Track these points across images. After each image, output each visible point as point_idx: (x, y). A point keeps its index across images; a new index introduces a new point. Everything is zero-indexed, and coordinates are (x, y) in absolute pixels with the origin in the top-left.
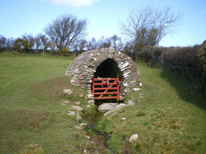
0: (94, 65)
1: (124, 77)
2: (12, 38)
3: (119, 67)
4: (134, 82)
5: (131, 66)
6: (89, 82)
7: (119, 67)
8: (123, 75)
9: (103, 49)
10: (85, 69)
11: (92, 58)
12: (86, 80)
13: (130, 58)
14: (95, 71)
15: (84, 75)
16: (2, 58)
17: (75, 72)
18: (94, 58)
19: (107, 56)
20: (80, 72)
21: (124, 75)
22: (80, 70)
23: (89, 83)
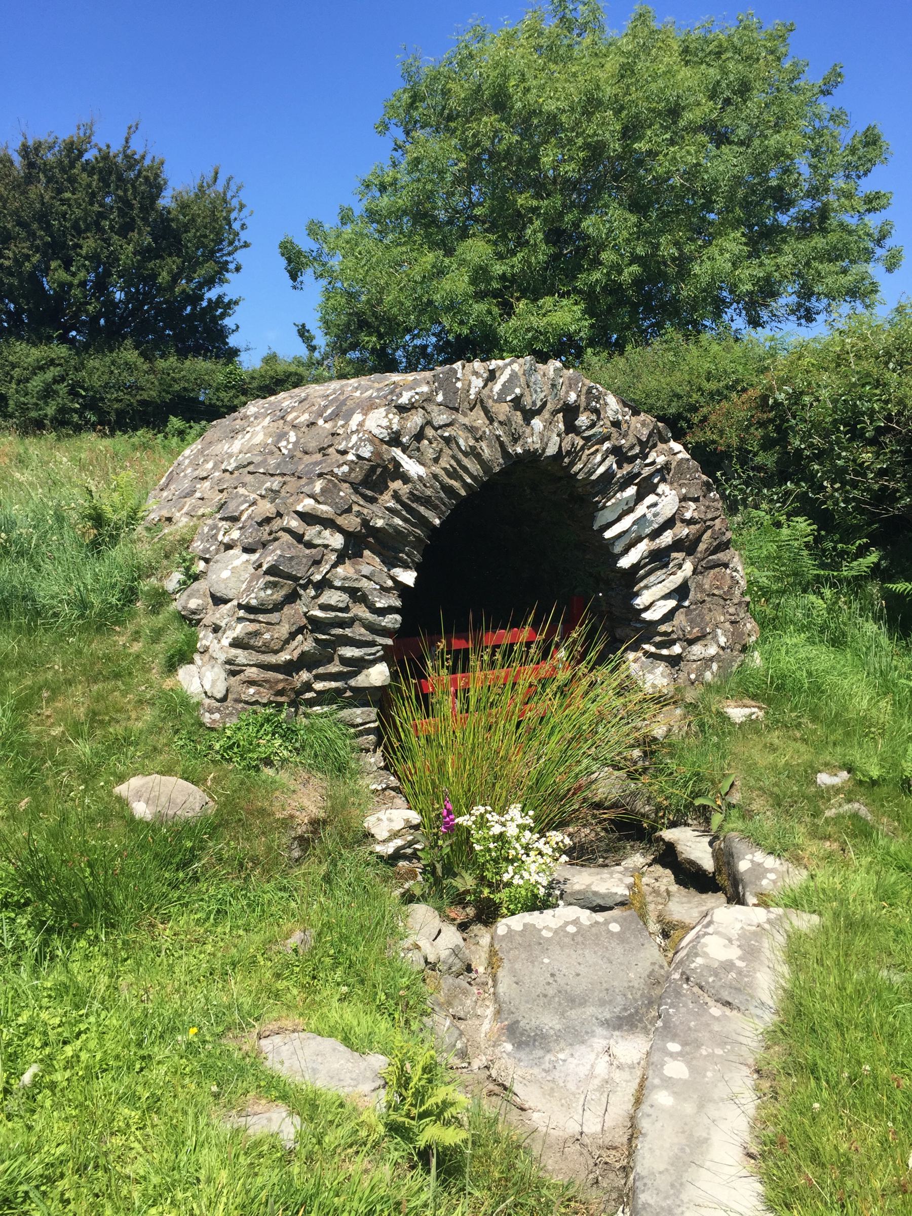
0: (398, 521)
1: (647, 616)
2: (644, 1135)
3: (608, 534)
4: (713, 650)
5: (690, 522)
6: (360, 681)
7: (608, 534)
8: (637, 594)
9: (476, 373)
10: (325, 568)
11: (377, 454)
12: (335, 668)
13: (685, 455)
14: (408, 577)
15: (312, 620)
16: (386, 379)
17: (221, 591)
18: (397, 453)
19: (515, 440)
20: (279, 596)
21: (640, 602)
22: (273, 571)
23: (363, 696)
